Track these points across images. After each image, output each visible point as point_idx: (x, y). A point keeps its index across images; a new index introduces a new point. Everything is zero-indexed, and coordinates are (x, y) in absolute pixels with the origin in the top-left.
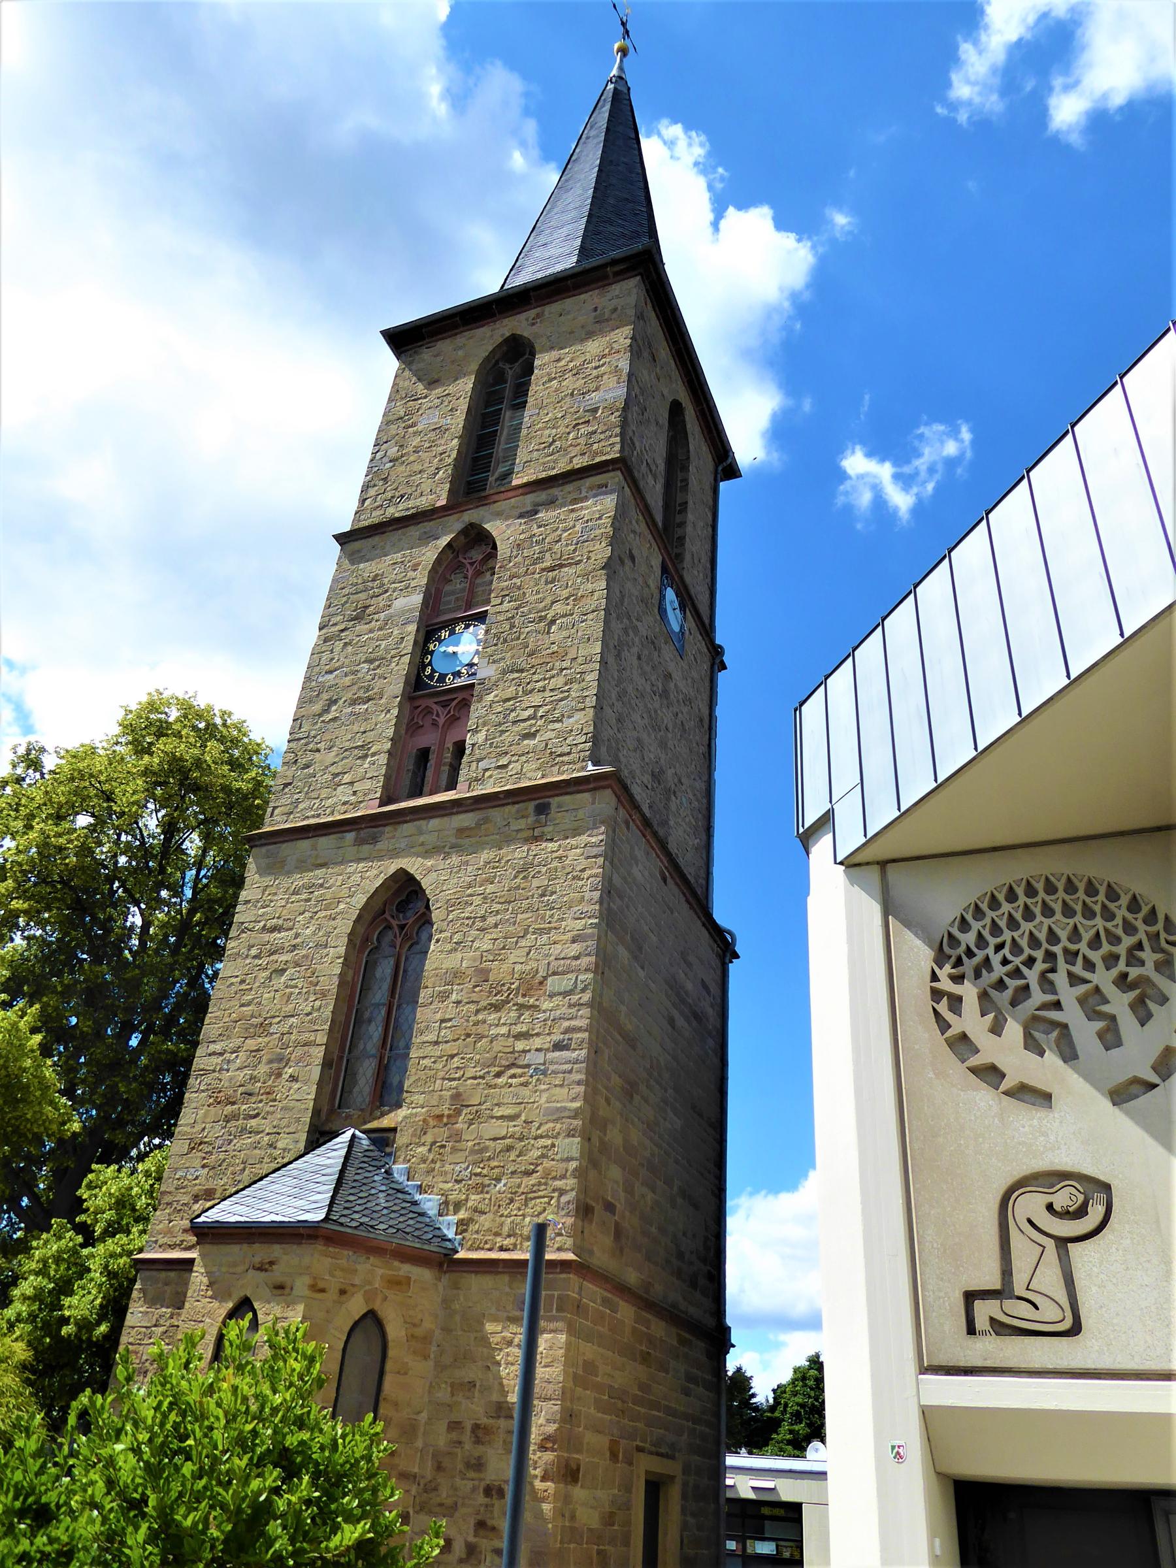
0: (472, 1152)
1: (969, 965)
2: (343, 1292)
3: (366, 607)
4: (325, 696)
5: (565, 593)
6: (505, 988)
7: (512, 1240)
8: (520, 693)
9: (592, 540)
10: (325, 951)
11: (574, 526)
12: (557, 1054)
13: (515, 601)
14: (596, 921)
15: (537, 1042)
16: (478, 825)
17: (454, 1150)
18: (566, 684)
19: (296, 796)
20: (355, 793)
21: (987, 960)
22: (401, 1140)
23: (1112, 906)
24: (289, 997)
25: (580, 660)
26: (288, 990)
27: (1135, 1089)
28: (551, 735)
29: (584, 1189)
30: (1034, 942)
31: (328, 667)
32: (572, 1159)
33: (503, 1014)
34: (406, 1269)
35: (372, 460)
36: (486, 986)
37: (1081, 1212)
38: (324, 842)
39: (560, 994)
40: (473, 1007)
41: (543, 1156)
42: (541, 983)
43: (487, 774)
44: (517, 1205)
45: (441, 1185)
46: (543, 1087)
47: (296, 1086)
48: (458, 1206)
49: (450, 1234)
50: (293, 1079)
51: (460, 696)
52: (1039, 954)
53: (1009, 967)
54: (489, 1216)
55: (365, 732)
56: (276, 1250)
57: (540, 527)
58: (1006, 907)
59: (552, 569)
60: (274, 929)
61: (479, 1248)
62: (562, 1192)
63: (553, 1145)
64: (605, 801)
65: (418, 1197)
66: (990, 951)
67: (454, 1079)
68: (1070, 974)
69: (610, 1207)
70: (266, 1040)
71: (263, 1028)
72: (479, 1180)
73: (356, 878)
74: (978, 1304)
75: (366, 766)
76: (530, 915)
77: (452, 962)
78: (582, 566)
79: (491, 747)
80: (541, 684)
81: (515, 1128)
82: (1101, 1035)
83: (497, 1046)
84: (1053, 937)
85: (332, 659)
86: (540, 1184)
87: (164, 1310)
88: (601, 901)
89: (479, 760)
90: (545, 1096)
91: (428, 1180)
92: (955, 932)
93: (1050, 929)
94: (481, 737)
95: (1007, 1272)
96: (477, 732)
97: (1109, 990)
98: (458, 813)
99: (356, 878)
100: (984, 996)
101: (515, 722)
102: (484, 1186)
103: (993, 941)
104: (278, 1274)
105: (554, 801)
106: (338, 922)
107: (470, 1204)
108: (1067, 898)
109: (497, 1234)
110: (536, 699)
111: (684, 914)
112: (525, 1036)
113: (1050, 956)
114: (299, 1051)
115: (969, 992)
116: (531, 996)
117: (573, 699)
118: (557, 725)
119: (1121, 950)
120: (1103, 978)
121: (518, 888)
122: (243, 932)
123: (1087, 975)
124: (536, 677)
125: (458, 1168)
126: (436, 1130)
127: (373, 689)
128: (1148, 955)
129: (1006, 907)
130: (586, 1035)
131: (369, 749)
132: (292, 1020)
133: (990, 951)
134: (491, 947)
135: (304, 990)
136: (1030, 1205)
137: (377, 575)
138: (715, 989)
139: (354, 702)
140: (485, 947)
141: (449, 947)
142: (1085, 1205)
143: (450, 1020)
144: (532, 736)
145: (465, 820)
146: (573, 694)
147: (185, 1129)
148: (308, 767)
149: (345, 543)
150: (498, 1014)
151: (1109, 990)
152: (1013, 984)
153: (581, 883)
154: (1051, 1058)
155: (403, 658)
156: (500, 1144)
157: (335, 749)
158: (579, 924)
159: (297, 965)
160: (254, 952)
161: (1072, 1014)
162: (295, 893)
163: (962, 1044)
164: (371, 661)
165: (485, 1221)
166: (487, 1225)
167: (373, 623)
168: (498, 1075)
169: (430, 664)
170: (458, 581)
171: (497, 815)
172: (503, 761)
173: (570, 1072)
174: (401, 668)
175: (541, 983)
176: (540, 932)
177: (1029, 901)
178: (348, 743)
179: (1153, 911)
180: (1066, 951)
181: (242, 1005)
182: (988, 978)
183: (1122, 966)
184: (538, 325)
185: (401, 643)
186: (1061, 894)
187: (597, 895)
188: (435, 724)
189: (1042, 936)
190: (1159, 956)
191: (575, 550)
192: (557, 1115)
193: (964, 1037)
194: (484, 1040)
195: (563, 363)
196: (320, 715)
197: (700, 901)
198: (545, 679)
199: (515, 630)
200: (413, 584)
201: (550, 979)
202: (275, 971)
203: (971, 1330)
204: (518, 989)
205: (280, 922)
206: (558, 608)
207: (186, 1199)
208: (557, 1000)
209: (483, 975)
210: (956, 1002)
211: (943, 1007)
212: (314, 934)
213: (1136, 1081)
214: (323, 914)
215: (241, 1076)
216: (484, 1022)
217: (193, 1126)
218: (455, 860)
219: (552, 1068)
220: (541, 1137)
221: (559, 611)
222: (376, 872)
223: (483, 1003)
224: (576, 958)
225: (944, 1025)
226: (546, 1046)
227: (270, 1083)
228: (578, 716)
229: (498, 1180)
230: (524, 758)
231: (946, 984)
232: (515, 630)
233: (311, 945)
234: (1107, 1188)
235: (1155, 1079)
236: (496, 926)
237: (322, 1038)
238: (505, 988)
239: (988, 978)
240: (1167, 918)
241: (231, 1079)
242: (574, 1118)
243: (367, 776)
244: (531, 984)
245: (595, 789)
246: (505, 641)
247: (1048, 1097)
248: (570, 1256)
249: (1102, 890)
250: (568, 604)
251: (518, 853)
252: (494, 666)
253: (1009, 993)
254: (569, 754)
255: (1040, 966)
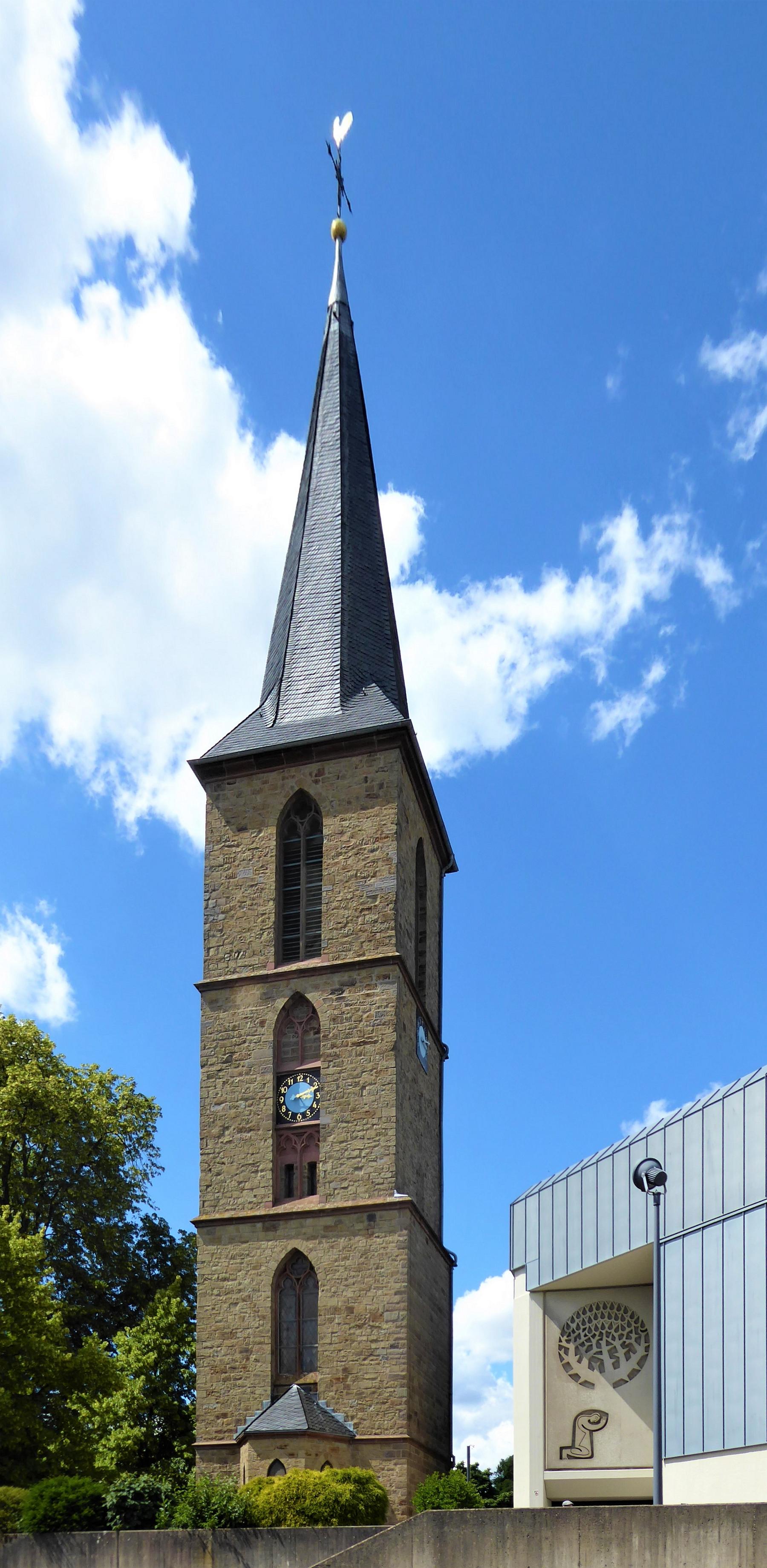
0: (356, 1394)
1: (573, 1336)
2: (317, 1455)
3: (233, 1053)
4: (219, 1123)
5: (369, 1066)
6: (363, 1317)
7: (380, 1430)
8: (349, 1138)
9: (383, 1025)
10: (260, 1293)
11: (370, 1010)
12: (392, 1350)
13: (337, 1066)
14: (406, 1284)
15: (382, 1344)
16: (336, 1225)
17: (348, 1394)
18: (377, 1135)
19: (217, 1195)
20: (255, 1196)
21: (579, 1334)
22: (321, 1388)
23: (625, 1315)
24: (244, 1319)
25: (384, 1119)
26: (242, 1315)
27: (623, 1382)
28: (372, 1170)
29: (409, 1409)
30: (596, 1328)
31: (215, 1100)
32: (404, 1397)
33: (363, 1330)
34: (337, 1444)
35: (206, 908)
36: (353, 1316)
37: (598, 1422)
38: (245, 1228)
39: (390, 1321)
40: (347, 1326)
41: (390, 1396)
42: (381, 1315)
43: (336, 1192)
44: (380, 1416)
45: (344, 1409)
46: (387, 1365)
47: (259, 1364)
48: (353, 1418)
49: (351, 1429)
50: (256, 1360)
51: (309, 1131)
52: (597, 1333)
53: (587, 1338)
54: (368, 1421)
55: (253, 1154)
56: (287, 1441)
57: (347, 1005)
58: (589, 1314)
59: (358, 1044)
60: (225, 1279)
61: (365, 1434)
62: (400, 1411)
63: (394, 1391)
64: (406, 1216)
65: (333, 1414)
66: (581, 1331)
67: (343, 1361)
68: (607, 1341)
69: (416, 1413)
70: (236, 1340)
71: (232, 1334)
72: (361, 1406)
73: (268, 1252)
74: (564, 1451)
75: (259, 1178)
76: (371, 1279)
77: (334, 1302)
78: (378, 1045)
79: (336, 1174)
80: (360, 1134)
81: (376, 1383)
82: (613, 1364)
83: (362, 1346)
84: (603, 1327)
85: (217, 1094)
86: (390, 1407)
87: (215, 1465)
88: (408, 1273)
89: (330, 1182)
90: (388, 1369)
91: (337, 1407)
92: (569, 1323)
93: (603, 1324)
94: (329, 1166)
95: (574, 1441)
96: (326, 1162)
97: (619, 1347)
98: (323, 1216)
99: (268, 1252)
100: (577, 1348)
101: (348, 1159)
102: (364, 1409)
103: (582, 1327)
104: (289, 1450)
105: (378, 1214)
106: (263, 1277)
107: (358, 1416)
108: (610, 1311)
109: (372, 1428)
110: (359, 1144)
111: (431, 1249)
112: (376, 1341)
113: (601, 1334)
114: (256, 1347)
115: (571, 1347)
116: (377, 1322)
117: (382, 1147)
118: (374, 1164)
119: (625, 1333)
120: (617, 1343)
121: (363, 1263)
122: (205, 1280)
123: (612, 1342)
124: (358, 1128)
125: (350, 1401)
126: (337, 1385)
127: (251, 1122)
128: (633, 1336)
129: (589, 1314)
130: (406, 1341)
131: (258, 1166)
132: (250, 1330)
133: (581, 1331)
134: (352, 1295)
135: (252, 1315)
136: (583, 1420)
137: (235, 1026)
138: (447, 1290)
139: (240, 1131)
140: (349, 1295)
141: (329, 1294)
142: (600, 1420)
143: (336, 1332)
144: (359, 1169)
145: (329, 1221)
146: (383, 1144)
147: (201, 1385)
148: (220, 1175)
149: (204, 991)
150: (361, 1330)
151: (619, 1347)
152: (587, 1344)
153: (396, 1263)
154: (596, 1372)
155: (268, 1100)
156: (369, 1391)
157: (235, 1164)
158: (398, 1286)
159: (244, 1300)
160: (215, 1292)
161: (605, 1357)
162: (233, 1258)
163: (567, 1366)
164: (246, 1100)
165: (366, 1423)
166: (368, 1425)
167: (240, 1068)
168: (365, 1359)
169: (284, 1103)
170: (291, 1035)
171: (346, 1219)
172: (345, 1184)
173: (399, 1359)
174: (268, 1107)
175: (381, 1315)
176: (378, 1288)
177: (597, 1312)
178: (243, 1161)
179: (638, 1318)
180: (607, 1332)
181: (217, 1322)
182: (579, 1342)
183: (624, 1339)
184: (321, 783)
185: (264, 1088)
186: (608, 1309)
187: (405, 1270)
188: (294, 1148)
189: (599, 1326)
190: (637, 1336)
191: (373, 1031)
192: (395, 1377)
193: (568, 1363)
194: (355, 1343)
195: (345, 838)
196: (219, 1137)
197: (435, 1236)
198: (363, 1130)
199: (340, 1090)
200: (263, 1038)
201: (385, 1314)
202: (231, 1303)
203: (561, 1458)
204: (369, 1318)
205: (227, 1275)
206: (365, 1077)
207: (212, 1418)
208: (390, 1324)
209: (350, 1310)
210: (567, 1350)
211: (562, 1352)
212: (250, 1283)
213: (622, 1380)
214: (253, 1272)
215: (226, 1359)
216: (354, 1334)
217: (205, 1383)
218: (325, 1245)
219: (391, 1356)
220: (388, 1387)
221: (367, 1080)
222: (280, 1249)
223: (352, 1325)
224: (398, 1303)
225: (562, 1359)
226: (387, 1346)
227: (244, 1362)
228: (386, 1159)
229: (370, 1406)
230: (356, 1184)
231: (564, 1344)
232: (340, 1090)
233: (250, 1290)
234: (607, 1414)
235: (627, 1379)
236: (354, 1284)
237: (268, 1340)
238: (363, 1317)
239: (579, 1342)
240: (642, 1321)
241: (221, 1361)
242: (403, 1379)
243: (261, 1185)
244: (376, 1316)
245: (400, 1209)
246: (335, 1098)
247: (593, 1385)
248: (406, 1436)
249: (623, 1309)
250: (372, 1075)
251: (360, 1242)
252: (330, 1116)
253: (585, 1348)
254: (383, 1183)
255: (597, 1338)
